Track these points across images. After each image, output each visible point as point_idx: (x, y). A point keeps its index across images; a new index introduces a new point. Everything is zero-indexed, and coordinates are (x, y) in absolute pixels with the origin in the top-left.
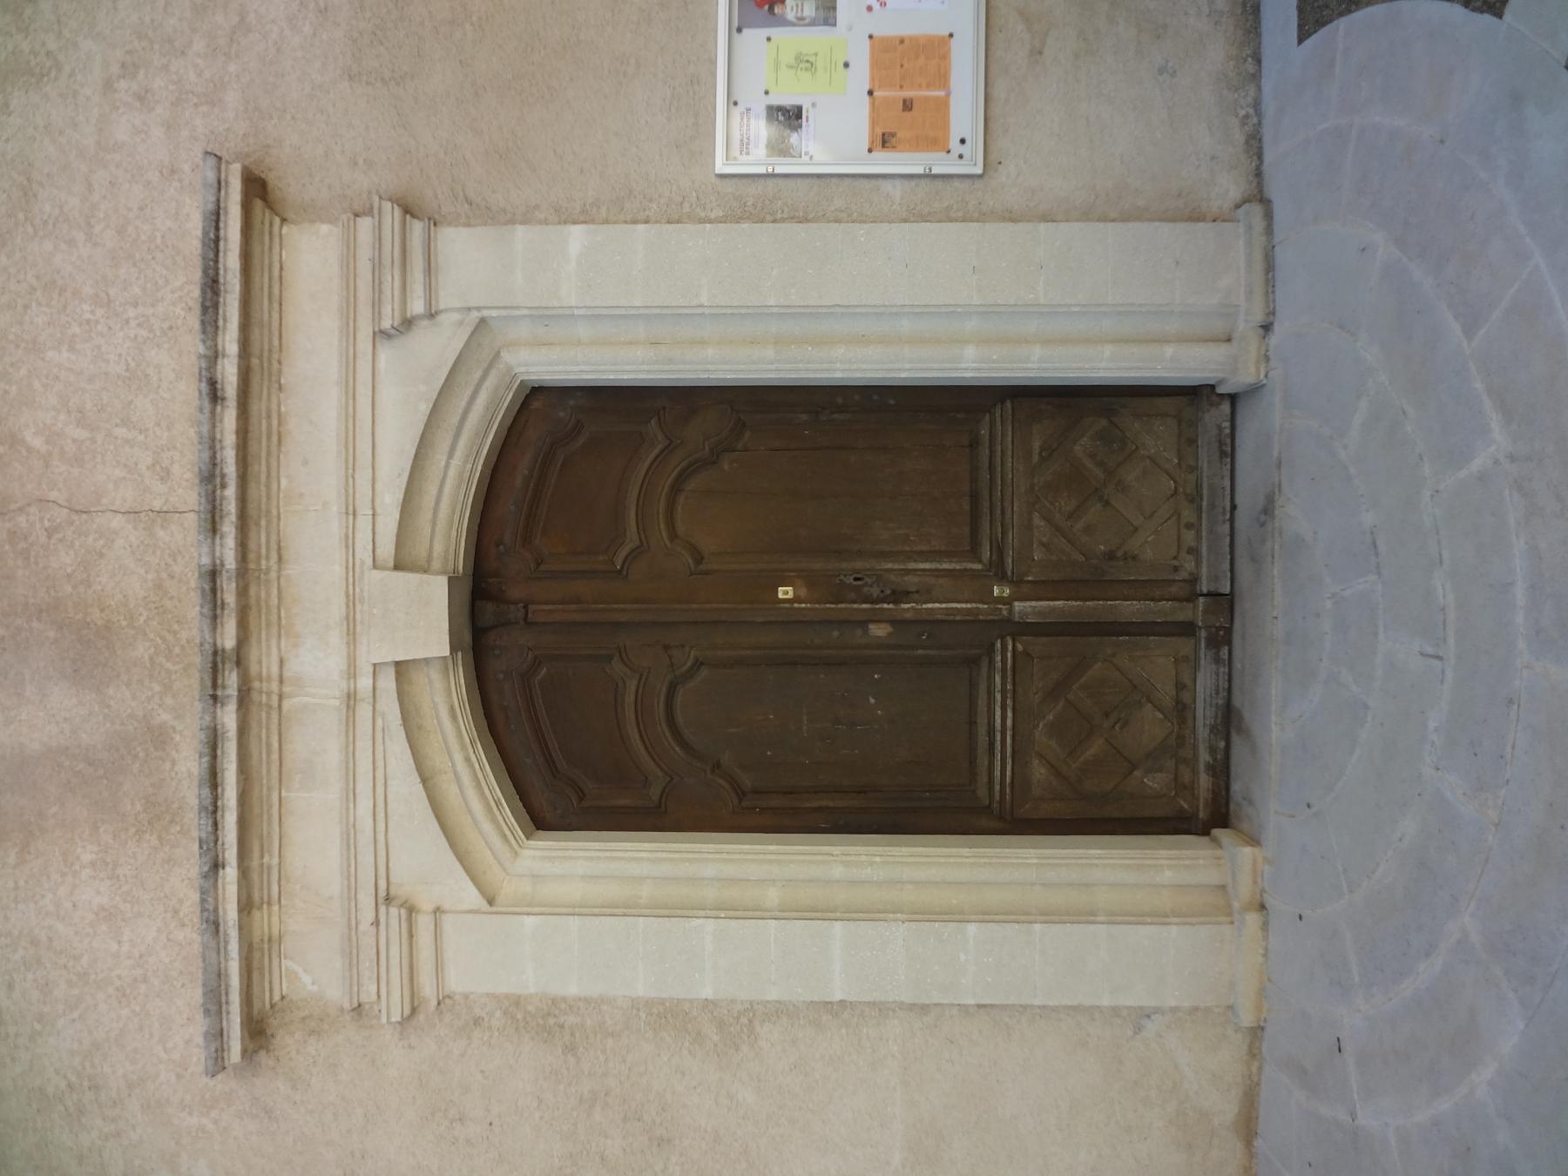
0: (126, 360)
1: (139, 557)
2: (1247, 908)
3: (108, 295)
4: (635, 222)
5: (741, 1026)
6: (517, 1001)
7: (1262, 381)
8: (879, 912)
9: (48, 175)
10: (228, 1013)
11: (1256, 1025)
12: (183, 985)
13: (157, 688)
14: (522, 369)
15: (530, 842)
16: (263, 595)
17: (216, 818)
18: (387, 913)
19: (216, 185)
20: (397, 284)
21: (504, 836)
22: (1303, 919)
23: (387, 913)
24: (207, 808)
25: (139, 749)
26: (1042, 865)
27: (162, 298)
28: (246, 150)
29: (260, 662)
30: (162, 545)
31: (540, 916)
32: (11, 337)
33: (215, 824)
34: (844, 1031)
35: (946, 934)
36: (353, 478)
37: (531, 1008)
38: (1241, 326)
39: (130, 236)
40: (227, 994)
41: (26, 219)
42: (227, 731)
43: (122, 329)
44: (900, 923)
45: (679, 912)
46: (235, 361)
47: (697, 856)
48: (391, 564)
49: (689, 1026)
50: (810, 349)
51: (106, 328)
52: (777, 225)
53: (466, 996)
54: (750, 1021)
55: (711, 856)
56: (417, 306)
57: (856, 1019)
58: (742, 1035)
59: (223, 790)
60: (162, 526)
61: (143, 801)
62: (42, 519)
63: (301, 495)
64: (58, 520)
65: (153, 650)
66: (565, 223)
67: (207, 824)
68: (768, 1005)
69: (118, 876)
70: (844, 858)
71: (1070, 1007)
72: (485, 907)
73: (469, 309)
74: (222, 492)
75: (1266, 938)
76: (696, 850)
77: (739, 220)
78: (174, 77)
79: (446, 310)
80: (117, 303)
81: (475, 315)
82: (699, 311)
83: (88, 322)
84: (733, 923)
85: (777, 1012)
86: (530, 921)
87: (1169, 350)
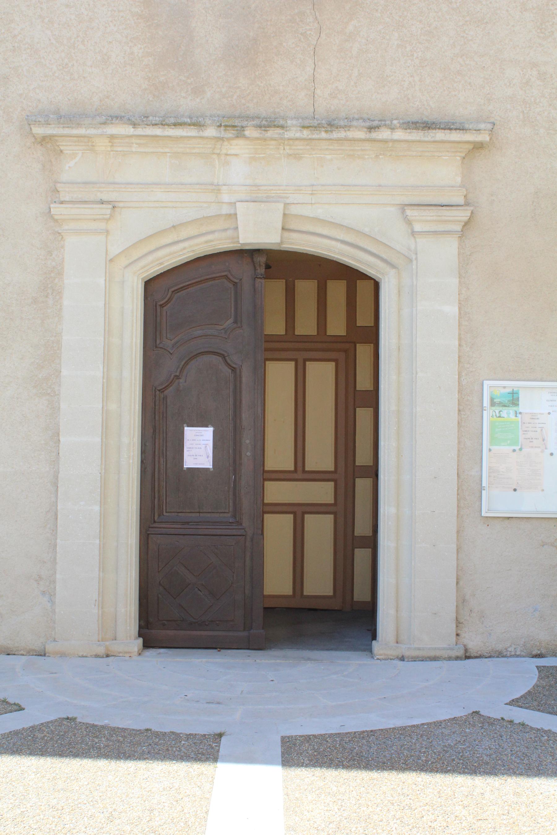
0: (392, 76)
1: (291, 82)
3: (426, 66)
4: (460, 339)
5: (46, 389)
6: (60, 274)
7: (376, 657)
9: (489, 33)
10: (58, 127)
11: (46, 652)
12: (69, 100)
13: (224, 90)
16: (271, 147)
17: (159, 124)
18: (107, 208)
19: (477, 129)
20: (429, 218)
21: (144, 267)
23: (107, 208)
24: (164, 121)
25: (192, 79)
27: (424, 95)
28: (500, 138)
29: (237, 145)
30: (297, 94)
31: (104, 286)
32: (405, 13)
33: (156, 125)
34: (43, 442)
35: (94, 495)
36: (331, 193)
37: (57, 280)
39: (456, 78)
40: (68, 127)
41: (466, 21)
42: (203, 131)
43: (408, 73)
44: (100, 471)
46: (389, 138)
48: (286, 213)
49: (47, 362)
50: (395, 428)
51: (409, 65)
52: (457, 412)
53: (63, 247)
54: (49, 394)
56: (418, 227)
57: (49, 448)
58: (41, 390)
59: (173, 129)
60: (307, 94)
61: (165, 81)
62: (311, 30)
64: (310, 39)
65: (243, 88)
66: (460, 303)
67: (156, 121)
68: (57, 404)
69: (126, 67)
71: (55, 559)
72: (109, 258)
73: (416, 254)
74: (323, 131)
75: (91, 656)
76: (136, 367)
77: (460, 392)
78: (538, 100)
79: (416, 242)
80: (422, 71)
81: (414, 257)
83: (413, 55)
84: (101, 386)
85: (54, 408)
86: (102, 281)
87: (392, 612)
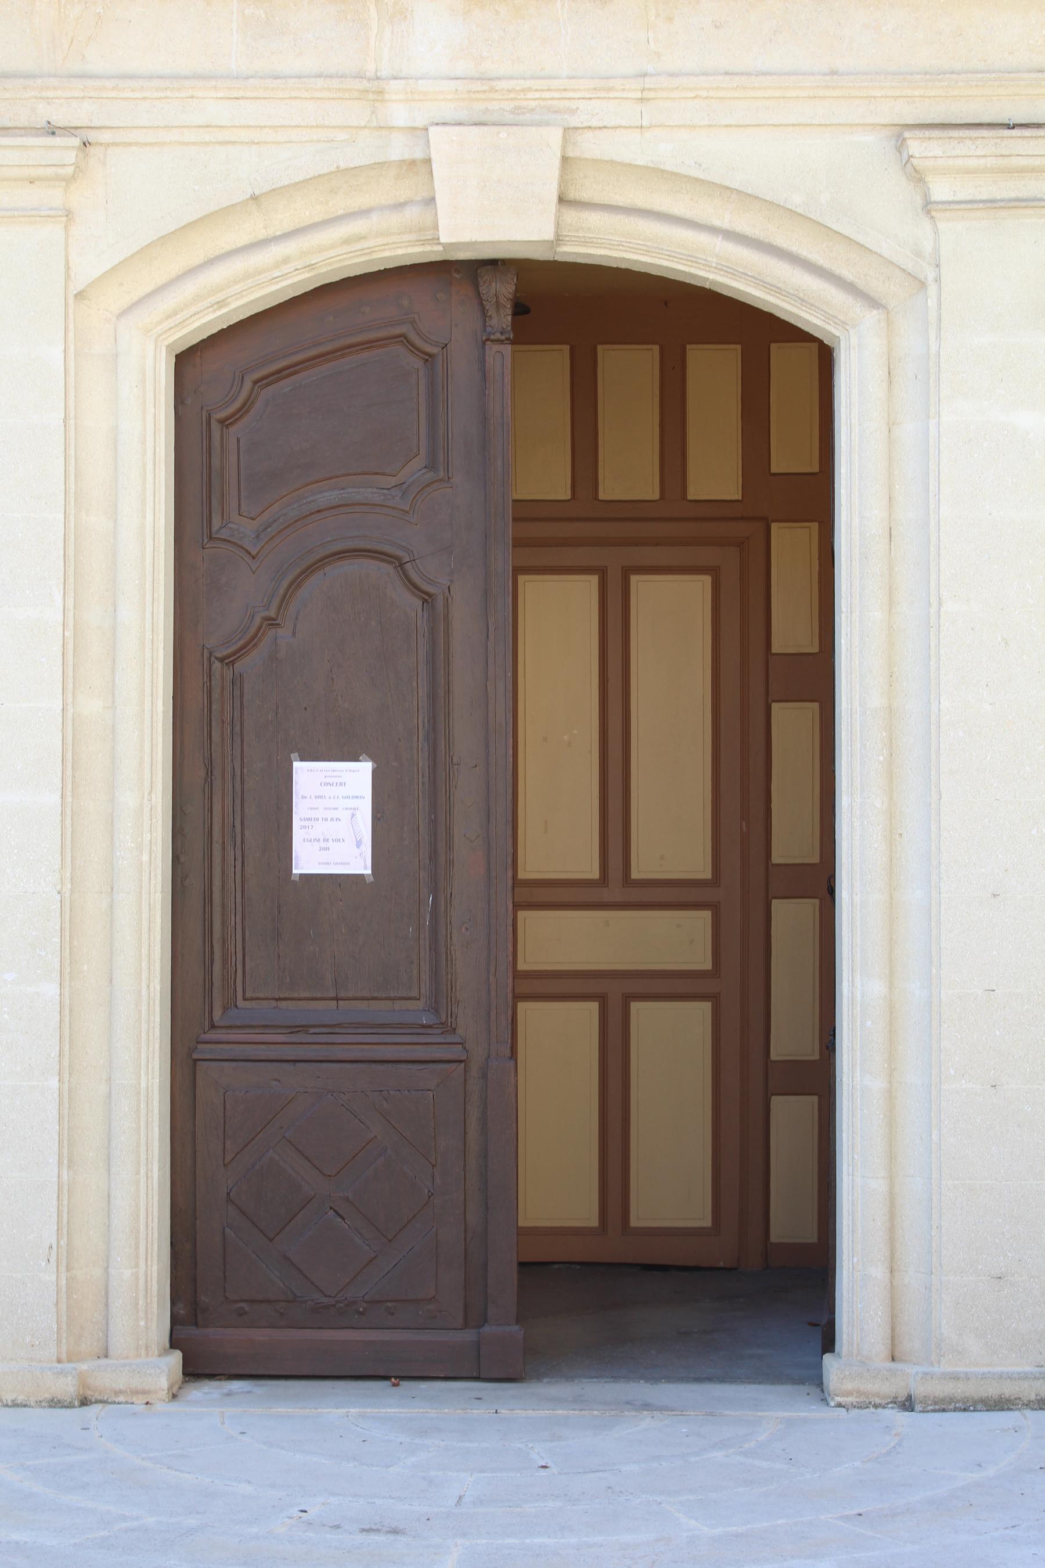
2: (82, 1378)
7: (833, 1399)
8: (73, 859)
14: (854, 341)
15: (164, 349)
18: (67, 148)
20: (972, 163)
22: (345, 841)
23: (67, 148)
26: (139, 1093)
36: (695, 97)
38: (911, 1370)
44: (59, 887)
45: (71, 571)
47: (149, 598)
50: (881, 758)
55: (148, 615)
56: (941, 190)
63: (670, 19)
70: (147, 810)
75: (39, 1403)
81: (931, 276)
82: (934, 600)
84: (57, 648)
